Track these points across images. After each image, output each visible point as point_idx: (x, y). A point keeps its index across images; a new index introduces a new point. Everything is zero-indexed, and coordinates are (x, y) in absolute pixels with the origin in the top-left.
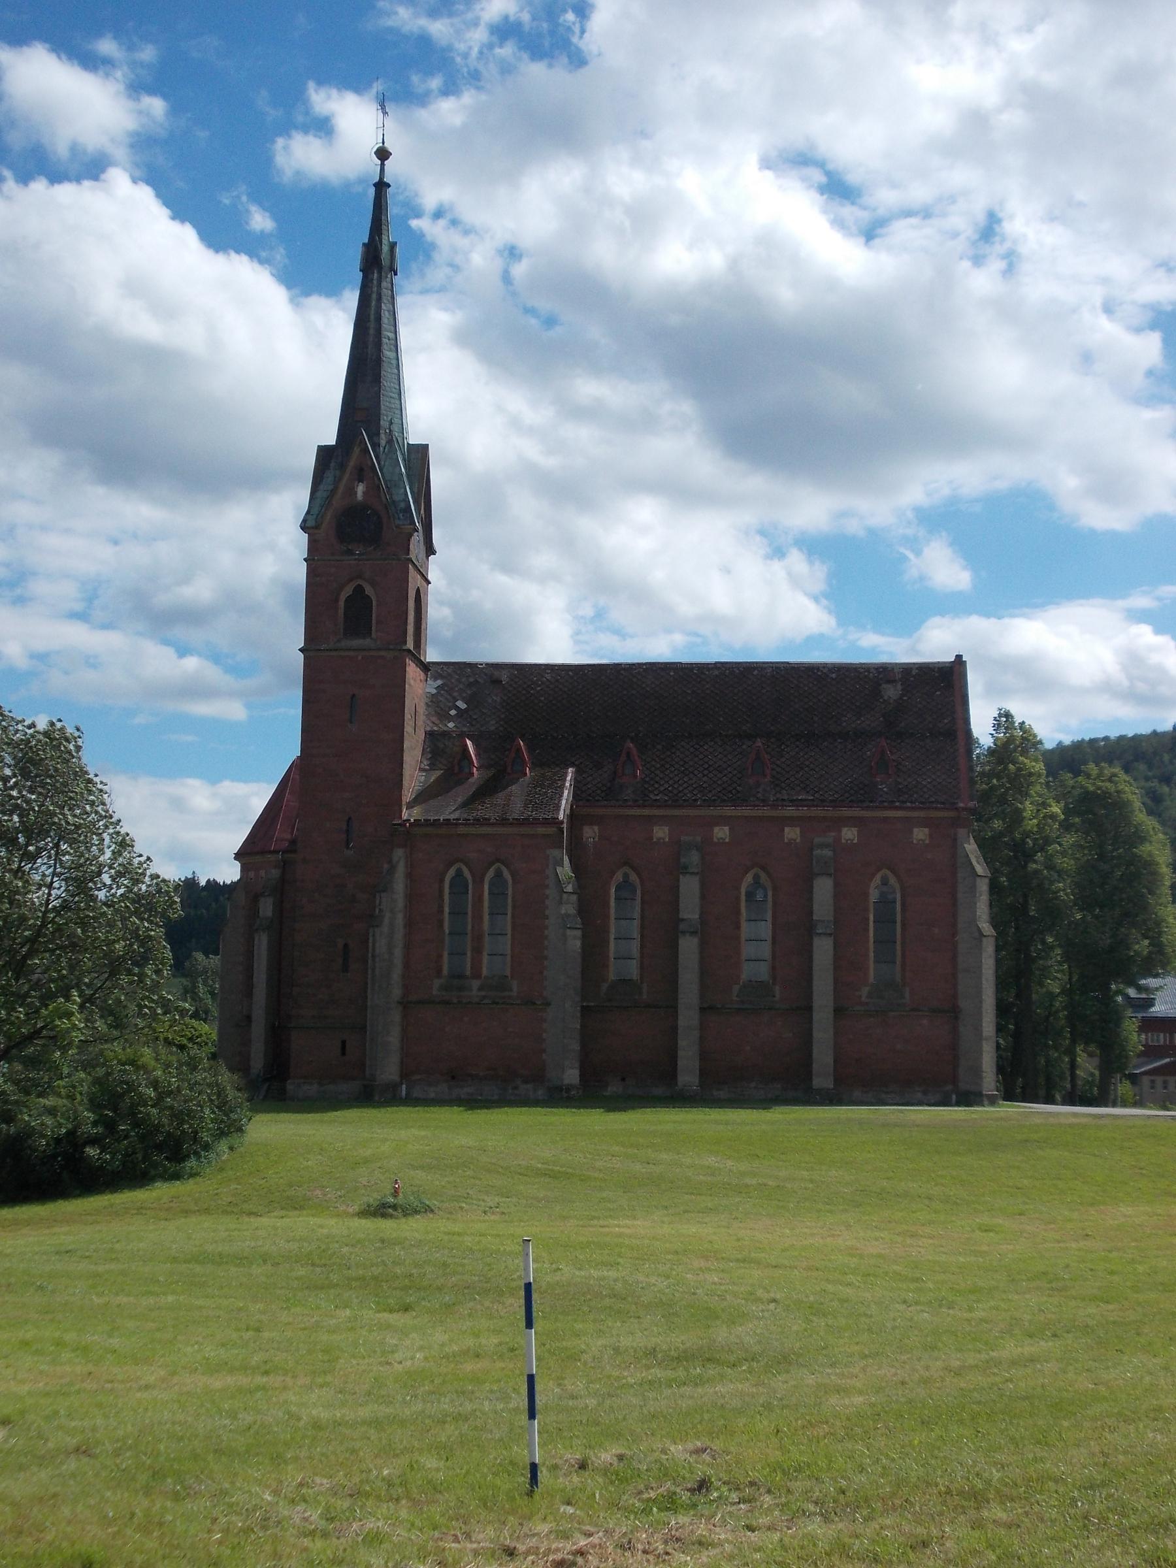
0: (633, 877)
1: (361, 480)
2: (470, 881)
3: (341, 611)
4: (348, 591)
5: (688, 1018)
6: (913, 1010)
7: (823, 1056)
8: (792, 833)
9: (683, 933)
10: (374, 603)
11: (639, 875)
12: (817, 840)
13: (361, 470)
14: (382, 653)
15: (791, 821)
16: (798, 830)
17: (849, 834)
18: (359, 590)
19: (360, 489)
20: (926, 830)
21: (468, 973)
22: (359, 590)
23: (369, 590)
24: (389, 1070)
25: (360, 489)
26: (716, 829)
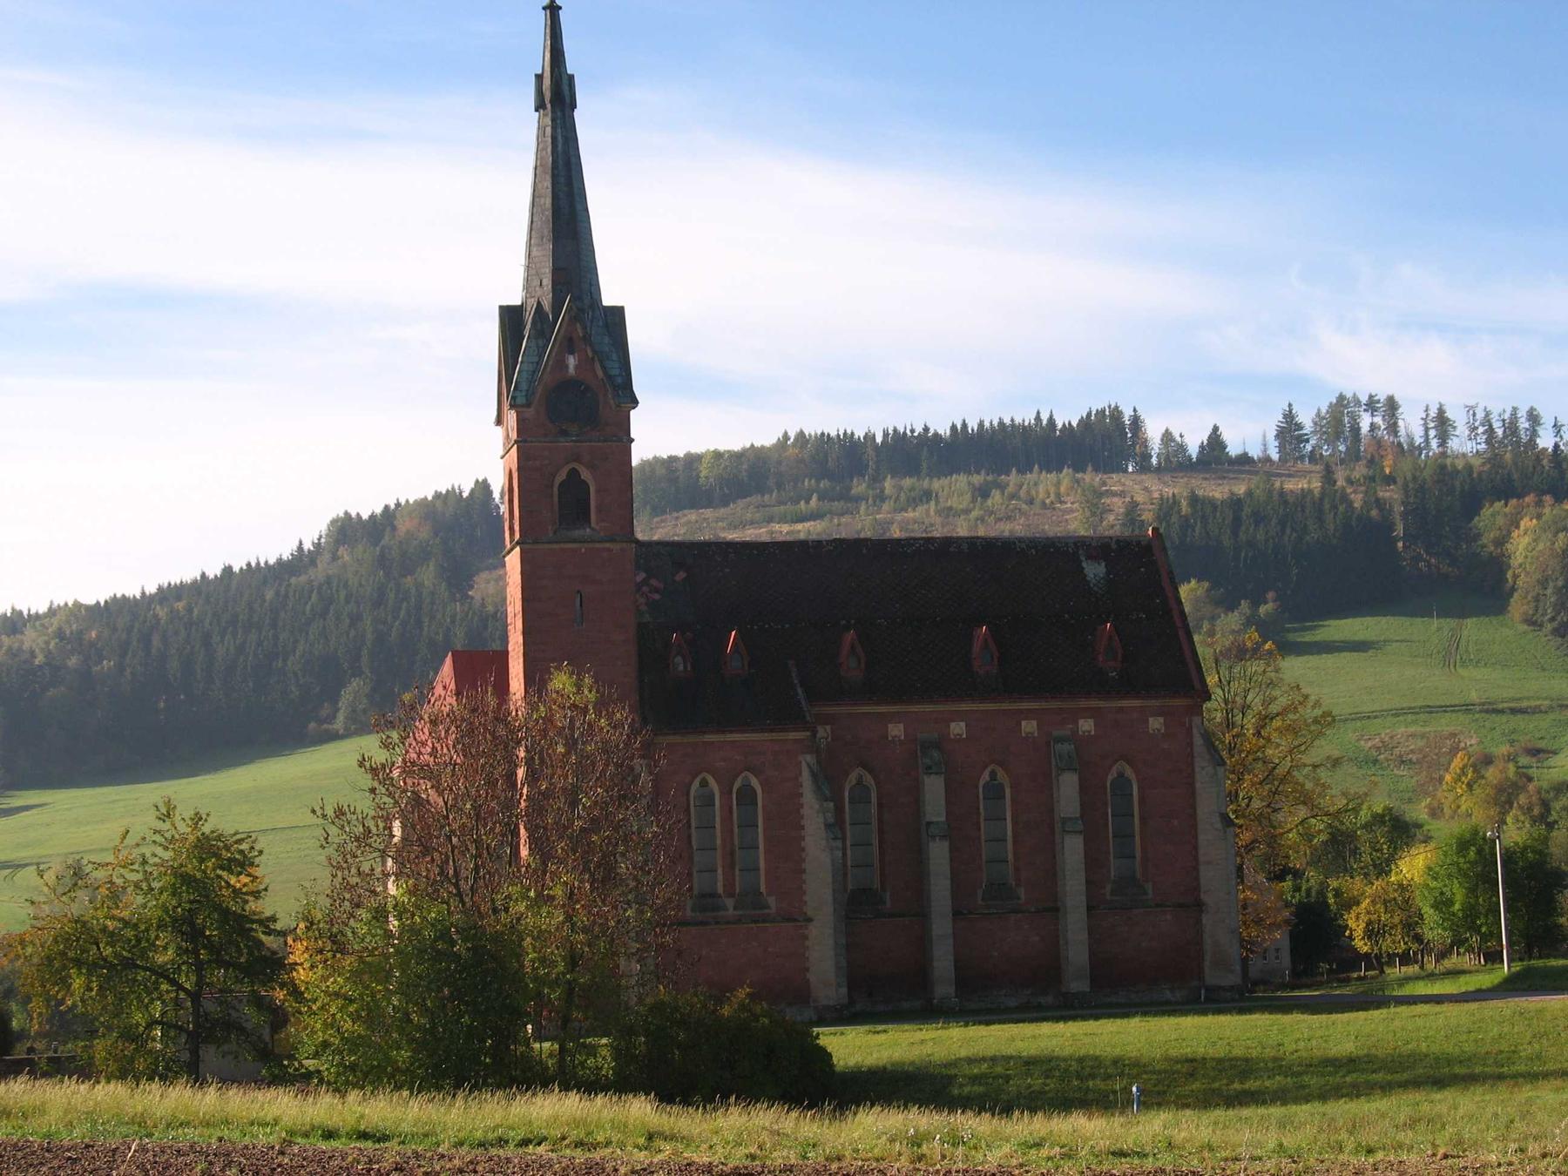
0: (869, 780)
1: (572, 352)
2: (759, 791)
3: (556, 499)
4: (562, 476)
5: (941, 925)
6: (1157, 905)
7: (943, 962)
8: (1029, 727)
9: (934, 837)
10: (592, 489)
11: (875, 778)
12: (1056, 733)
13: (570, 340)
14: (607, 545)
15: (1029, 714)
16: (1034, 723)
17: (1086, 726)
18: (574, 473)
19: (572, 361)
20: (1161, 720)
21: (720, 890)
22: (574, 473)
23: (585, 475)
24: (944, 989)
25: (572, 361)
26: (953, 725)
